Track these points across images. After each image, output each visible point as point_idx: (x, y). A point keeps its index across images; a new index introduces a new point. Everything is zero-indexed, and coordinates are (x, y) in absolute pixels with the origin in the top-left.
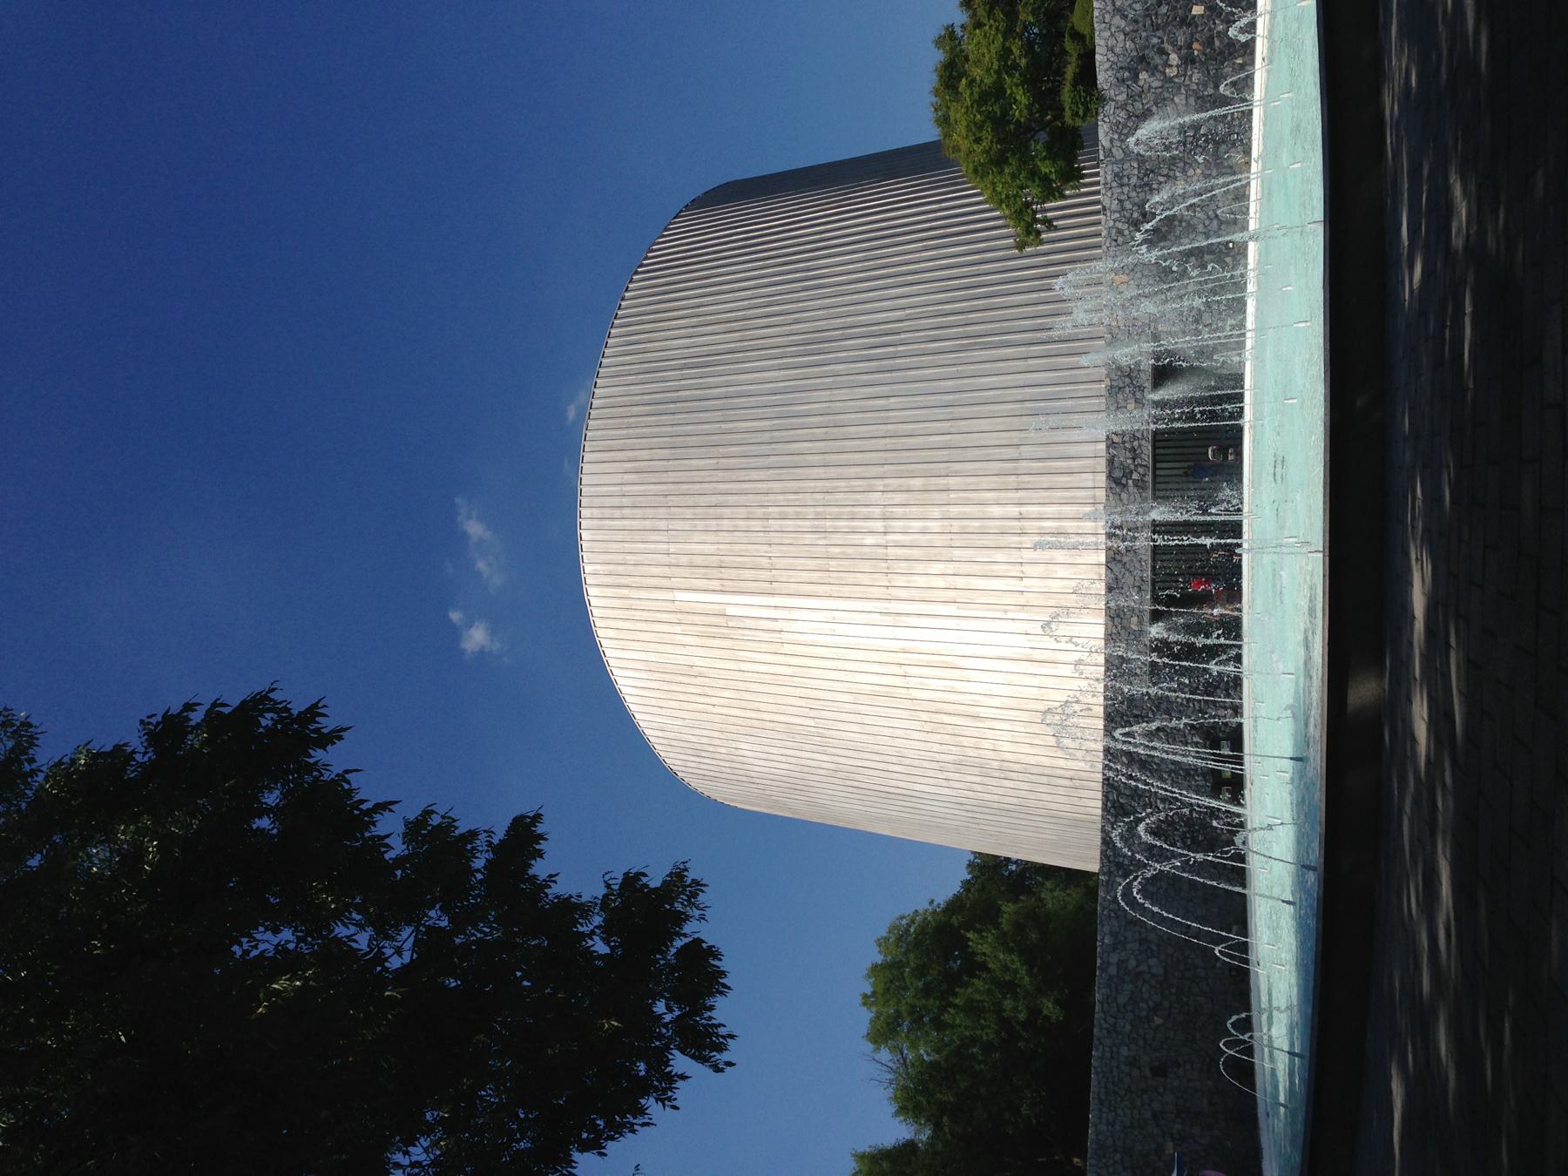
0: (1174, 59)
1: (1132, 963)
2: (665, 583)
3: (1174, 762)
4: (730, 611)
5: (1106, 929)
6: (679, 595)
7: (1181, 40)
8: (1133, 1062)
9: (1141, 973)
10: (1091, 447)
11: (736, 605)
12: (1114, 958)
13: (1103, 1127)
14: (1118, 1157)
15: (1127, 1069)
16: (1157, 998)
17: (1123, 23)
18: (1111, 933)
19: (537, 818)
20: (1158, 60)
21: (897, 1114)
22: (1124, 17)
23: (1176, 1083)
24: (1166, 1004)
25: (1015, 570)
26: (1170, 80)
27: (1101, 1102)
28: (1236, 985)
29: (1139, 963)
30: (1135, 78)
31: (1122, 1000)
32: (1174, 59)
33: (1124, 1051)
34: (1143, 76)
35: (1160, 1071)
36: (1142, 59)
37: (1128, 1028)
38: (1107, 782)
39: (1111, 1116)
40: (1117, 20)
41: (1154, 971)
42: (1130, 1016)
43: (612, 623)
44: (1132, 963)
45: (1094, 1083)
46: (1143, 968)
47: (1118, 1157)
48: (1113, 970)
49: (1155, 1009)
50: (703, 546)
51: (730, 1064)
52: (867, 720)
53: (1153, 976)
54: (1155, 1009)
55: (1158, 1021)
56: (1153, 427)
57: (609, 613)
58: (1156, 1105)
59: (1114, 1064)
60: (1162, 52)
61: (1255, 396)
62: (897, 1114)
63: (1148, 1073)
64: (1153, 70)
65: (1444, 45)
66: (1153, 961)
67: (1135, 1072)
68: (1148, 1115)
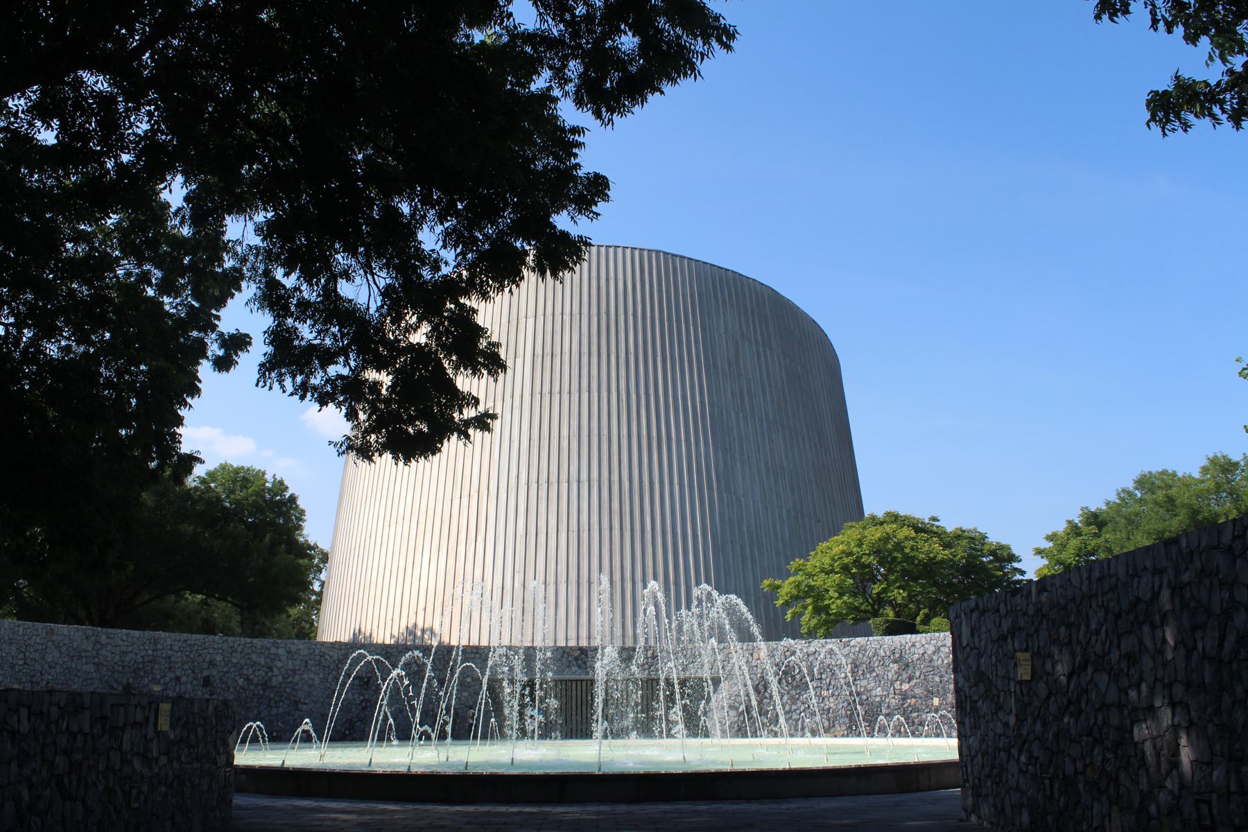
0: (905, 687)
1: (279, 664)
5: (301, 647)
7: (917, 691)
8: (212, 664)
9: (271, 669)
10: (584, 633)
12: (281, 652)
13: (169, 642)
14: (150, 652)
15: (208, 659)
16: (255, 680)
17: (929, 652)
19: (726, 36)
20: (905, 676)
22: (934, 653)
26: (892, 684)
27: (185, 641)
28: (280, 735)
29: (279, 669)
30: (895, 662)
31: (254, 657)
32: (905, 687)
33: (219, 658)
34: (895, 666)
35: (207, 682)
36: (907, 666)
37: (234, 660)
39: (176, 648)
40: (931, 649)
42: (243, 661)
44: (279, 664)
45: (198, 636)
46: (276, 672)
47: (150, 652)
48: (273, 650)
49: (247, 679)
50: (569, 341)
51: (598, 215)
54: (247, 679)
55: (241, 681)
56: (662, 677)
58: (184, 679)
59: (211, 651)
60: (910, 679)
61: (744, 746)
63: (206, 673)
64: (898, 674)
65: (560, 809)
66: (280, 678)
67: (206, 665)
68: (178, 673)
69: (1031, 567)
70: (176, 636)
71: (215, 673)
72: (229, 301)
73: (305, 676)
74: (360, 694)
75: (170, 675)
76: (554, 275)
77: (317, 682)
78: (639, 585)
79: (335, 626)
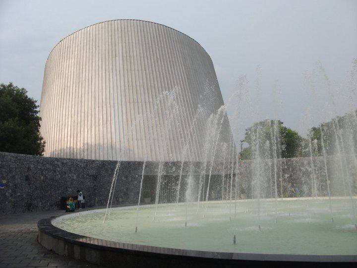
2: (124, 41)
3: (336, 196)
4: (117, 58)
6: (120, 45)
8: (29, 169)
9: (55, 171)
11: (119, 60)
15: (27, 166)
18: (67, 163)
21: (11, 85)
23: (24, 184)
24: (47, 180)
25: (139, 138)
27: (17, 157)
33: (32, 166)
35: (27, 178)
38: (140, 164)
41: (57, 176)
42: (43, 168)
43: (110, 26)
45: (23, 155)
52: (86, 95)
53: (55, 176)
57: (97, 29)
58: (17, 177)
62: (11, 85)
63: (27, 174)
66: (59, 176)
69: (47, 154)
70: (12, 154)
71: (31, 174)
72: (40, 122)
73: (70, 175)
74: (93, 183)
75: (10, 175)
76: (36, 107)
77: (75, 178)
78: (155, 99)
79: (47, 154)
